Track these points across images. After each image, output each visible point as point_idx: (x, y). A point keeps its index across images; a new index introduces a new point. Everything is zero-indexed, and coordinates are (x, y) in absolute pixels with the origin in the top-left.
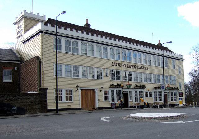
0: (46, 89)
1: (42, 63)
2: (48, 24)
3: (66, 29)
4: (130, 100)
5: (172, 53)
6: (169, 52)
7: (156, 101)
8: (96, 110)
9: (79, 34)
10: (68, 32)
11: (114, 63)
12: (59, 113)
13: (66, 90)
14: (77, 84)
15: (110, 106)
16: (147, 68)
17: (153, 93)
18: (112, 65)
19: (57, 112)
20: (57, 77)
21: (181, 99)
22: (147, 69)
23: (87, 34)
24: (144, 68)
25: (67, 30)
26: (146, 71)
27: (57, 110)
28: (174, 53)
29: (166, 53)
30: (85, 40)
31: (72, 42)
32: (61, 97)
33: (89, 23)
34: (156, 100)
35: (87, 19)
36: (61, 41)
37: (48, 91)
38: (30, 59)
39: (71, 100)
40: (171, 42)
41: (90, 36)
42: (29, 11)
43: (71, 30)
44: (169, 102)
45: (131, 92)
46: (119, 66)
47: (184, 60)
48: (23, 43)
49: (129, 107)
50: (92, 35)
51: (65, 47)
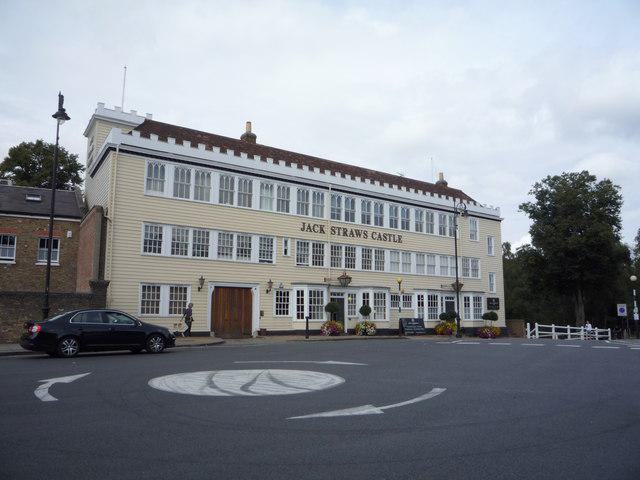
2: (185, 142)
3: (264, 159)
9: (229, 158)
11: (306, 225)
13: (172, 288)
15: (396, 327)
18: (303, 230)
22: (400, 241)
26: (397, 246)
28: (475, 203)
31: (343, 200)
41: (256, 164)
42: (110, 105)
43: (311, 169)
46: (322, 231)
50: (235, 154)
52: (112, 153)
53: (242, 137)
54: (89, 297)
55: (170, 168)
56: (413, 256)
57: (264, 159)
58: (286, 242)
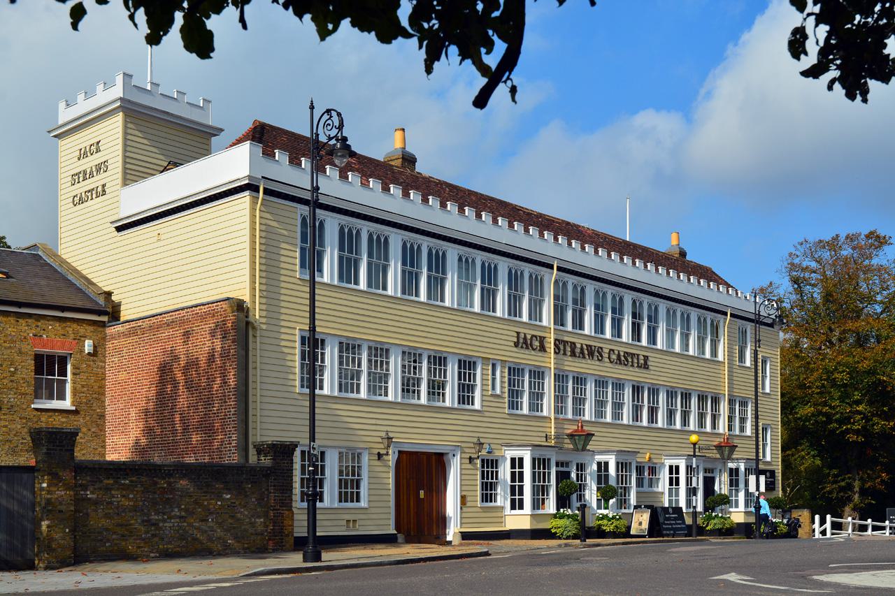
11: (522, 335)
16: (646, 358)
18: (516, 345)
20: (313, 397)
22: (646, 366)
36: (360, 234)
41: (411, 207)
48: (119, 229)
54: (266, 473)
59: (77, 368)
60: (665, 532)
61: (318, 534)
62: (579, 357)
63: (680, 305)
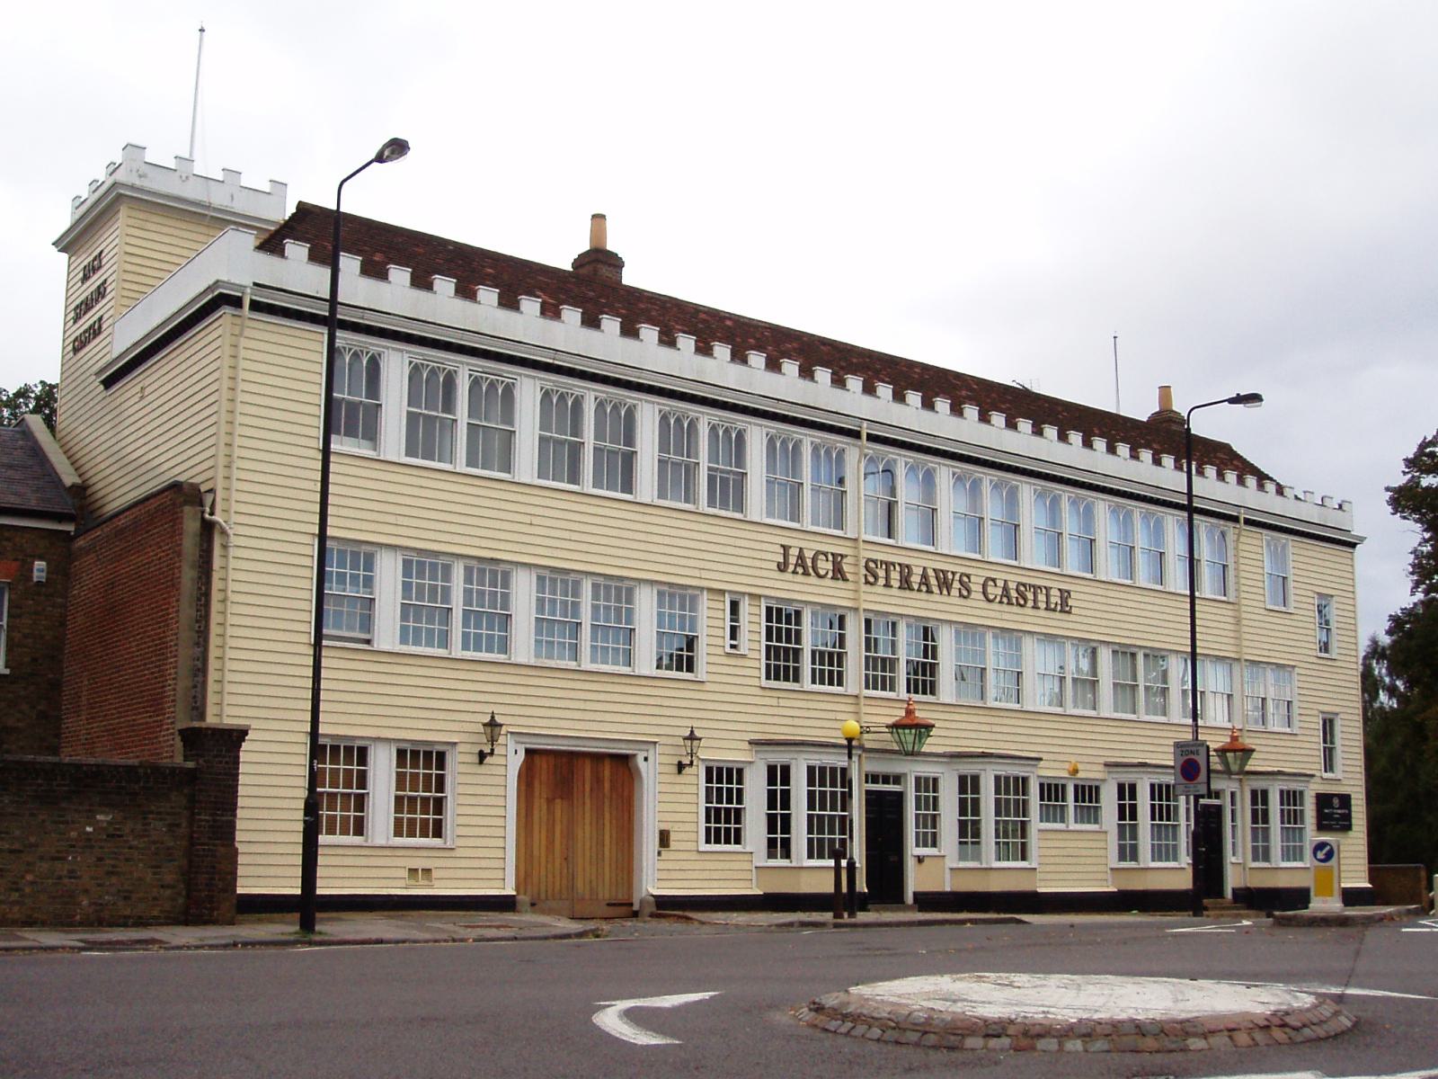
0: (234, 738)
1: (224, 532)
3: (509, 302)
4: (922, 841)
5: (1261, 487)
6: (1241, 481)
7: (787, 855)
8: (635, 914)
9: (526, 325)
10: (441, 305)
11: (794, 552)
12: (329, 927)
13: (401, 754)
14: (489, 709)
16: (1065, 595)
17: (748, 776)
18: (782, 568)
19: (307, 925)
21: (1329, 856)
22: (1065, 607)
23: (591, 321)
24: (1042, 597)
25: (428, 286)
27: (308, 907)
28: (1280, 490)
29: (1212, 487)
30: (571, 372)
32: (361, 802)
33: (610, 247)
34: (1128, 851)
35: (598, 218)
37: (248, 753)
38: (147, 499)
39: (438, 833)
40: (1254, 398)
41: (607, 344)
44: (1238, 870)
45: (928, 785)
46: (838, 573)
47: (1362, 539)
49: (909, 899)
50: (661, 342)
51: (412, 419)
52: (227, 310)
53: (580, 262)
55: (529, 390)
56: (1105, 656)
57: (466, 291)
58: (735, 607)
59: (18, 607)
60: (844, 890)
61: (319, 892)
62: (919, 590)
63: (903, 452)
